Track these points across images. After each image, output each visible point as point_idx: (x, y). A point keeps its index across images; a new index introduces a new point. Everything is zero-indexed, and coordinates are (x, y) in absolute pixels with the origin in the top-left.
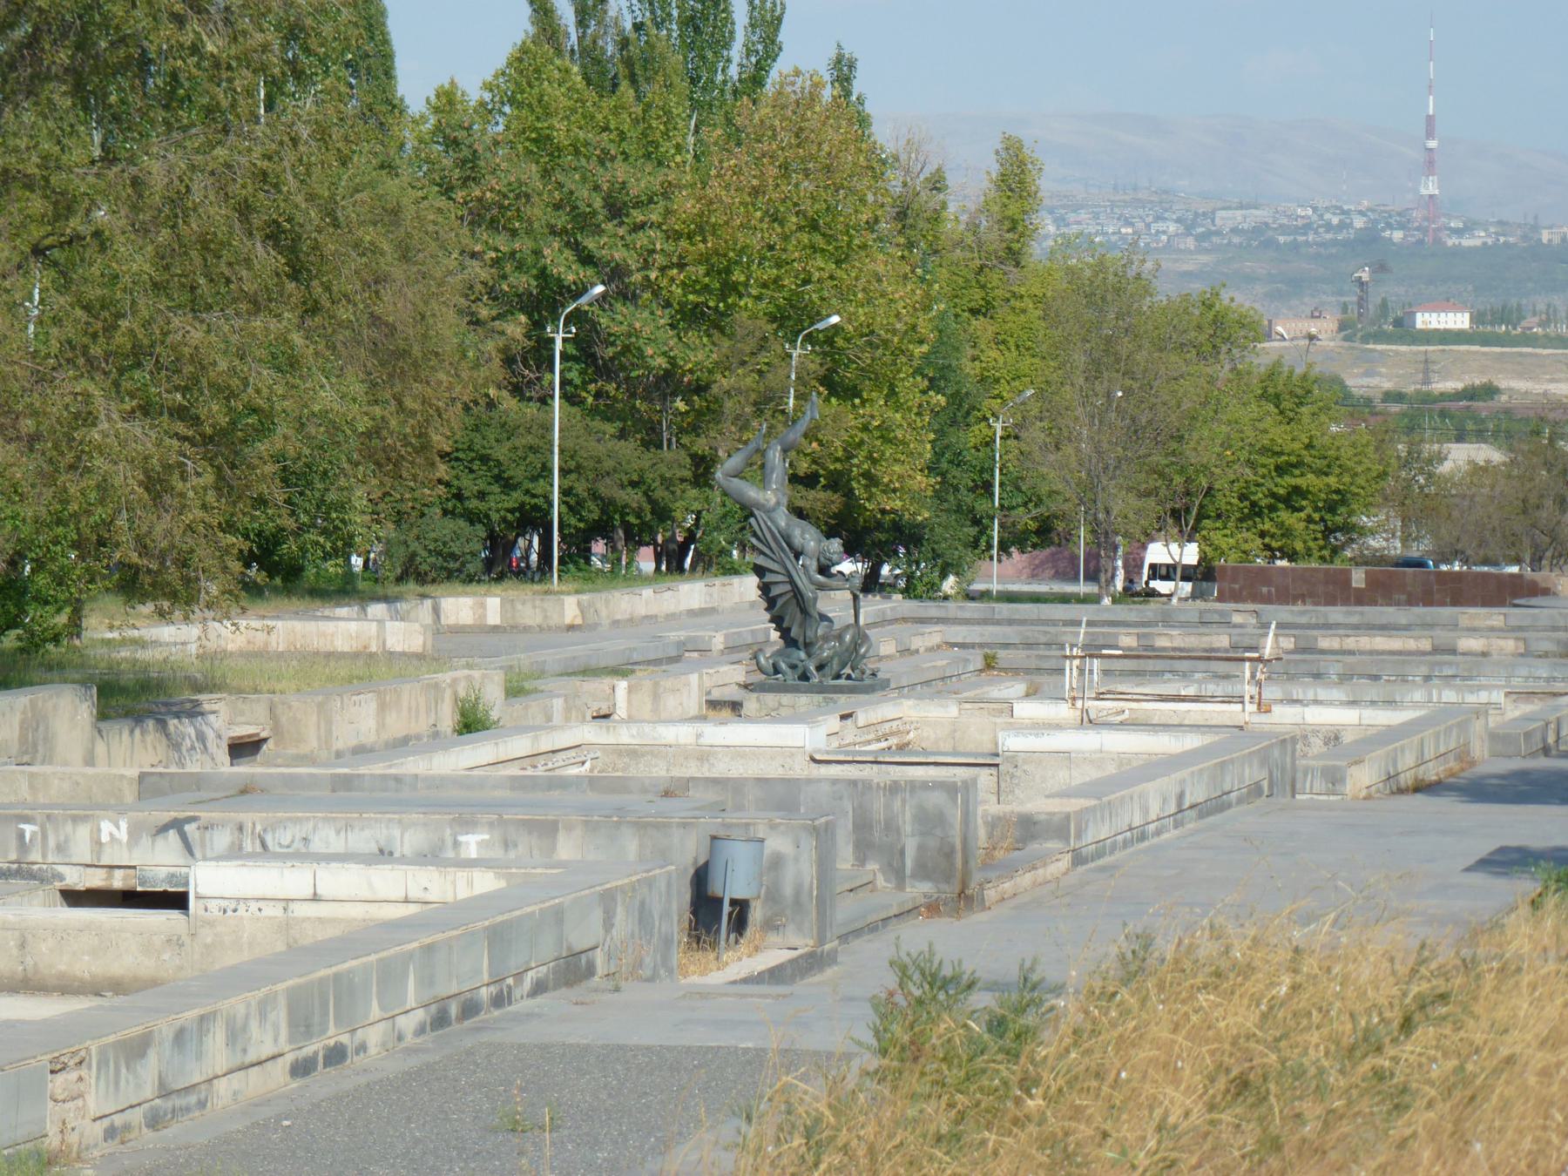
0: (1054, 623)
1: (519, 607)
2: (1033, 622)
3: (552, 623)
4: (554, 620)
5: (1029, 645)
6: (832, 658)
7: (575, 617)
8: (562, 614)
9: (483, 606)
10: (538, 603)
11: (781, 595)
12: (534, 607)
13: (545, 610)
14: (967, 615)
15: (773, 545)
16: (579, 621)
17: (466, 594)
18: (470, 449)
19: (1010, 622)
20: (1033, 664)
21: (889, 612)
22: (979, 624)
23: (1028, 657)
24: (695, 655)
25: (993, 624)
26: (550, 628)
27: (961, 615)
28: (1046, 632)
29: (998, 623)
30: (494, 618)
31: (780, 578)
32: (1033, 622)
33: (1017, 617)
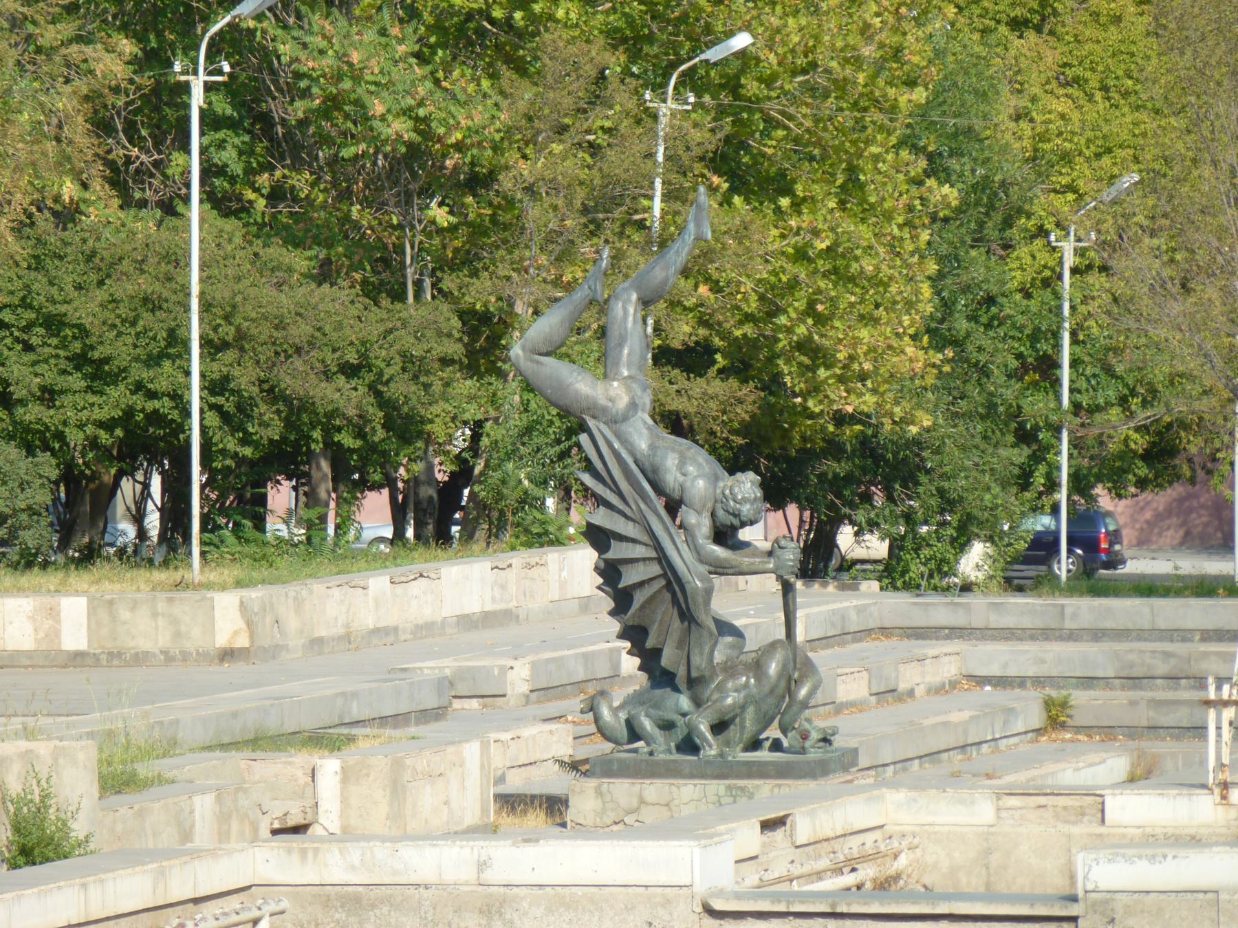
0: (1183, 635)
1: (124, 614)
2: (1140, 635)
3: (189, 646)
4: (195, 640)
5: (1133, 681)
6: (743, 708)
7: (236, 633)
8: (210, 627)
9: (53, 613)
10: (161, 606)
11: (641, 584)
12: (155, 615)
13: (175, 621)
14: (1009, 621)
15: (624, 486)
16: (243, 642)
17: (20, 591)
18: (25, 304)
19: (1098, 635)
20: (1143, 717)
21: (853, 615)
22: (1033, 638)
23: (1133, 703)
24: (474, 704)
25: (1061, 638)
26: (185, 656)
27: (996, 620)
28: (1167, 655)
29: (1072, 636)
30: (74, 638)
31: (639, 551)
32: (1140, 635)
33: (1109, 624)
